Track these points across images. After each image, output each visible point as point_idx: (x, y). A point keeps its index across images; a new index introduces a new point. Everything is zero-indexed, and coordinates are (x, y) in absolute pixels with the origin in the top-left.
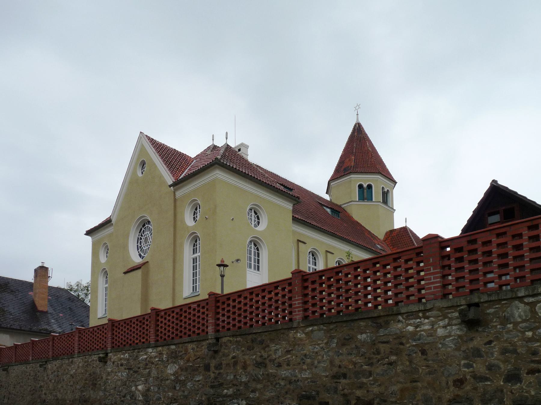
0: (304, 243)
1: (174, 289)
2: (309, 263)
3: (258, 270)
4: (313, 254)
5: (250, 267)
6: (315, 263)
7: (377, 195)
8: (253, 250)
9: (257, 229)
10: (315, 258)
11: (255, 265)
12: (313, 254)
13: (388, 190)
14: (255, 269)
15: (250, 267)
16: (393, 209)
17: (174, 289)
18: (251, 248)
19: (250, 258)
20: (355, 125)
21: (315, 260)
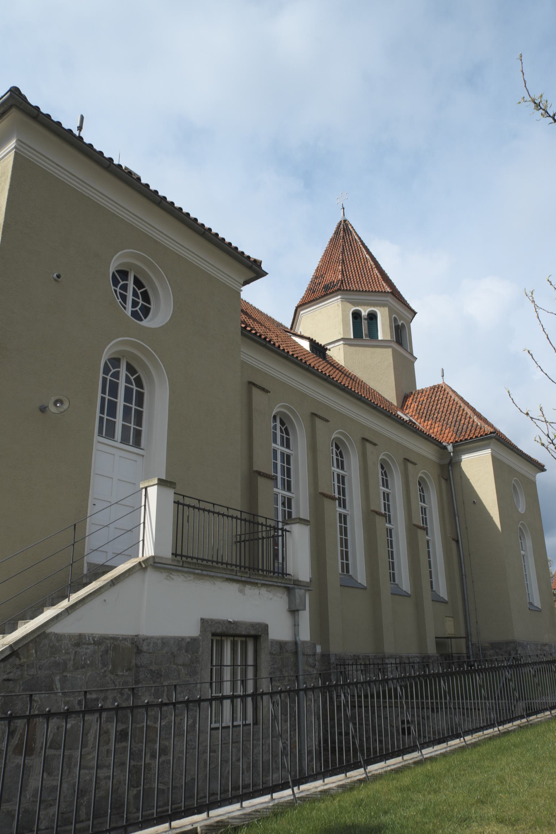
0: (266, 391)
1: (355, 588)
2: (275, 441)
3: (137, 443)
4: (283, 421)
5: (111, 434)
6: (288, 440)
7: (383, 331)
8: (122, 384)
9: (145, 323)
10: (286, 429)
11: (125, 429)
12: (283, 421)
13: (402, 324)
14: (125, 440)
15: (111, 434)
16: (412, 354)
17: (355, 588)
18: (116, 375)
19: (112, 407)
20: (340, 223)
21: (287, 434)
